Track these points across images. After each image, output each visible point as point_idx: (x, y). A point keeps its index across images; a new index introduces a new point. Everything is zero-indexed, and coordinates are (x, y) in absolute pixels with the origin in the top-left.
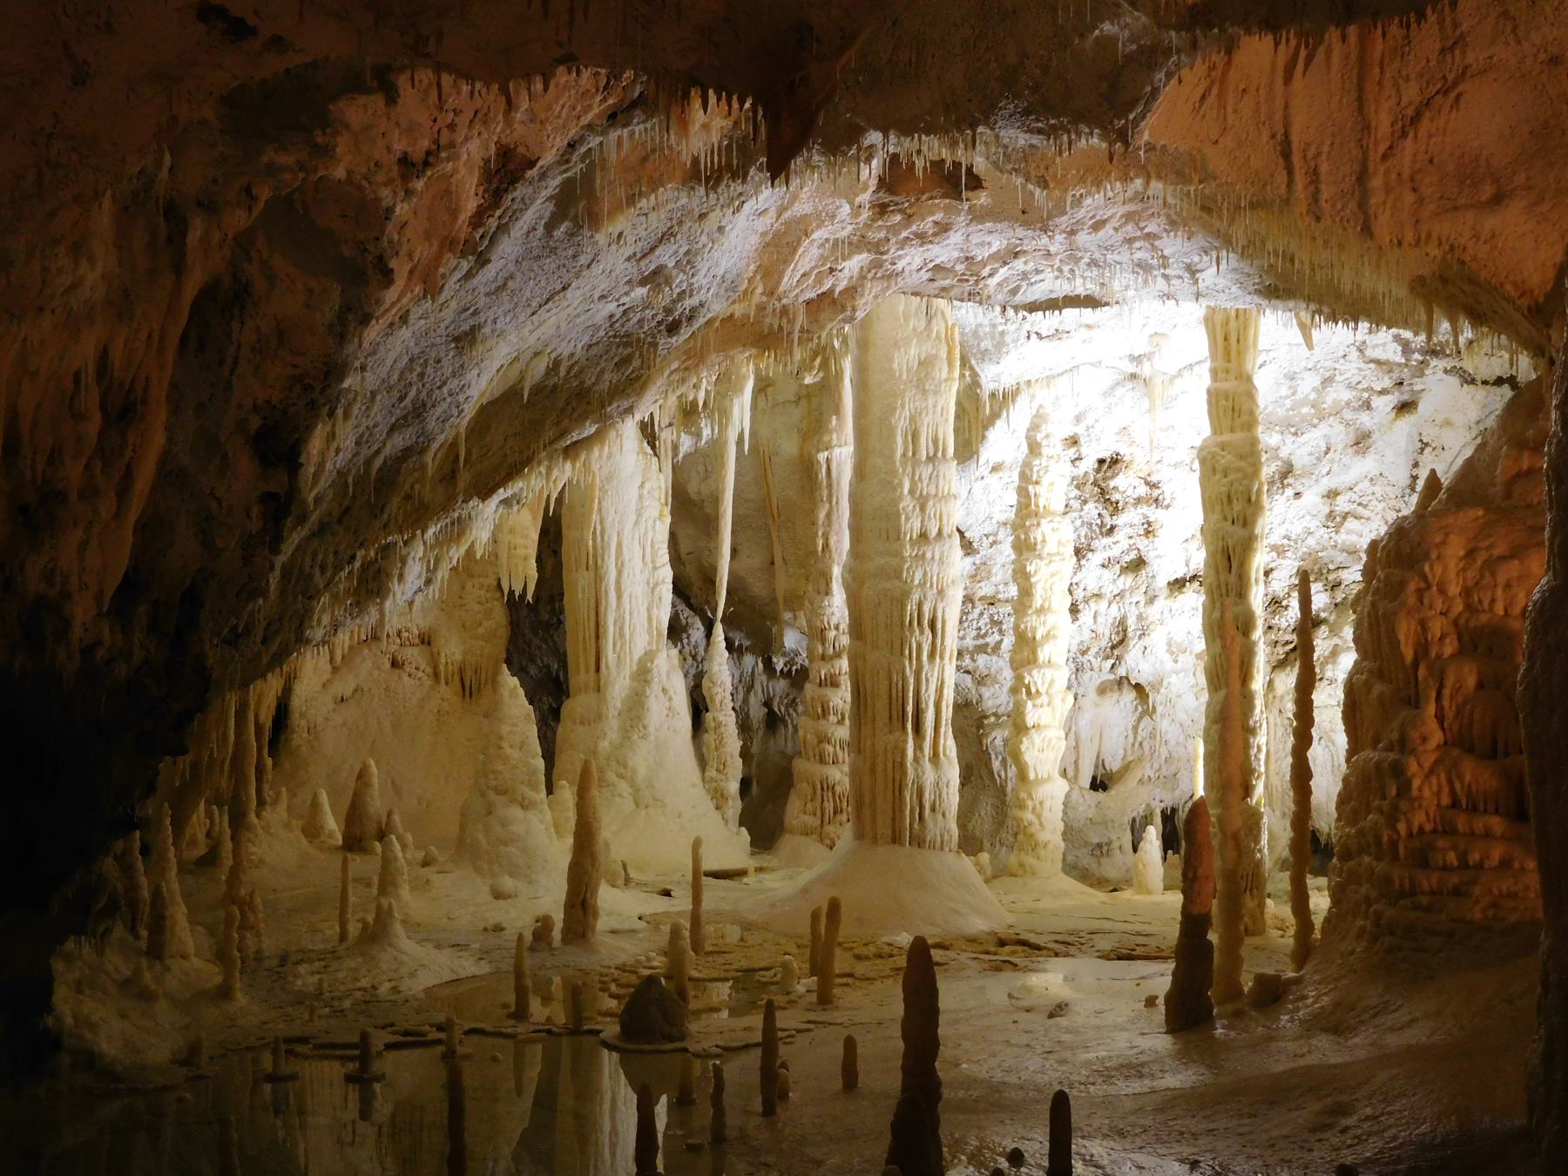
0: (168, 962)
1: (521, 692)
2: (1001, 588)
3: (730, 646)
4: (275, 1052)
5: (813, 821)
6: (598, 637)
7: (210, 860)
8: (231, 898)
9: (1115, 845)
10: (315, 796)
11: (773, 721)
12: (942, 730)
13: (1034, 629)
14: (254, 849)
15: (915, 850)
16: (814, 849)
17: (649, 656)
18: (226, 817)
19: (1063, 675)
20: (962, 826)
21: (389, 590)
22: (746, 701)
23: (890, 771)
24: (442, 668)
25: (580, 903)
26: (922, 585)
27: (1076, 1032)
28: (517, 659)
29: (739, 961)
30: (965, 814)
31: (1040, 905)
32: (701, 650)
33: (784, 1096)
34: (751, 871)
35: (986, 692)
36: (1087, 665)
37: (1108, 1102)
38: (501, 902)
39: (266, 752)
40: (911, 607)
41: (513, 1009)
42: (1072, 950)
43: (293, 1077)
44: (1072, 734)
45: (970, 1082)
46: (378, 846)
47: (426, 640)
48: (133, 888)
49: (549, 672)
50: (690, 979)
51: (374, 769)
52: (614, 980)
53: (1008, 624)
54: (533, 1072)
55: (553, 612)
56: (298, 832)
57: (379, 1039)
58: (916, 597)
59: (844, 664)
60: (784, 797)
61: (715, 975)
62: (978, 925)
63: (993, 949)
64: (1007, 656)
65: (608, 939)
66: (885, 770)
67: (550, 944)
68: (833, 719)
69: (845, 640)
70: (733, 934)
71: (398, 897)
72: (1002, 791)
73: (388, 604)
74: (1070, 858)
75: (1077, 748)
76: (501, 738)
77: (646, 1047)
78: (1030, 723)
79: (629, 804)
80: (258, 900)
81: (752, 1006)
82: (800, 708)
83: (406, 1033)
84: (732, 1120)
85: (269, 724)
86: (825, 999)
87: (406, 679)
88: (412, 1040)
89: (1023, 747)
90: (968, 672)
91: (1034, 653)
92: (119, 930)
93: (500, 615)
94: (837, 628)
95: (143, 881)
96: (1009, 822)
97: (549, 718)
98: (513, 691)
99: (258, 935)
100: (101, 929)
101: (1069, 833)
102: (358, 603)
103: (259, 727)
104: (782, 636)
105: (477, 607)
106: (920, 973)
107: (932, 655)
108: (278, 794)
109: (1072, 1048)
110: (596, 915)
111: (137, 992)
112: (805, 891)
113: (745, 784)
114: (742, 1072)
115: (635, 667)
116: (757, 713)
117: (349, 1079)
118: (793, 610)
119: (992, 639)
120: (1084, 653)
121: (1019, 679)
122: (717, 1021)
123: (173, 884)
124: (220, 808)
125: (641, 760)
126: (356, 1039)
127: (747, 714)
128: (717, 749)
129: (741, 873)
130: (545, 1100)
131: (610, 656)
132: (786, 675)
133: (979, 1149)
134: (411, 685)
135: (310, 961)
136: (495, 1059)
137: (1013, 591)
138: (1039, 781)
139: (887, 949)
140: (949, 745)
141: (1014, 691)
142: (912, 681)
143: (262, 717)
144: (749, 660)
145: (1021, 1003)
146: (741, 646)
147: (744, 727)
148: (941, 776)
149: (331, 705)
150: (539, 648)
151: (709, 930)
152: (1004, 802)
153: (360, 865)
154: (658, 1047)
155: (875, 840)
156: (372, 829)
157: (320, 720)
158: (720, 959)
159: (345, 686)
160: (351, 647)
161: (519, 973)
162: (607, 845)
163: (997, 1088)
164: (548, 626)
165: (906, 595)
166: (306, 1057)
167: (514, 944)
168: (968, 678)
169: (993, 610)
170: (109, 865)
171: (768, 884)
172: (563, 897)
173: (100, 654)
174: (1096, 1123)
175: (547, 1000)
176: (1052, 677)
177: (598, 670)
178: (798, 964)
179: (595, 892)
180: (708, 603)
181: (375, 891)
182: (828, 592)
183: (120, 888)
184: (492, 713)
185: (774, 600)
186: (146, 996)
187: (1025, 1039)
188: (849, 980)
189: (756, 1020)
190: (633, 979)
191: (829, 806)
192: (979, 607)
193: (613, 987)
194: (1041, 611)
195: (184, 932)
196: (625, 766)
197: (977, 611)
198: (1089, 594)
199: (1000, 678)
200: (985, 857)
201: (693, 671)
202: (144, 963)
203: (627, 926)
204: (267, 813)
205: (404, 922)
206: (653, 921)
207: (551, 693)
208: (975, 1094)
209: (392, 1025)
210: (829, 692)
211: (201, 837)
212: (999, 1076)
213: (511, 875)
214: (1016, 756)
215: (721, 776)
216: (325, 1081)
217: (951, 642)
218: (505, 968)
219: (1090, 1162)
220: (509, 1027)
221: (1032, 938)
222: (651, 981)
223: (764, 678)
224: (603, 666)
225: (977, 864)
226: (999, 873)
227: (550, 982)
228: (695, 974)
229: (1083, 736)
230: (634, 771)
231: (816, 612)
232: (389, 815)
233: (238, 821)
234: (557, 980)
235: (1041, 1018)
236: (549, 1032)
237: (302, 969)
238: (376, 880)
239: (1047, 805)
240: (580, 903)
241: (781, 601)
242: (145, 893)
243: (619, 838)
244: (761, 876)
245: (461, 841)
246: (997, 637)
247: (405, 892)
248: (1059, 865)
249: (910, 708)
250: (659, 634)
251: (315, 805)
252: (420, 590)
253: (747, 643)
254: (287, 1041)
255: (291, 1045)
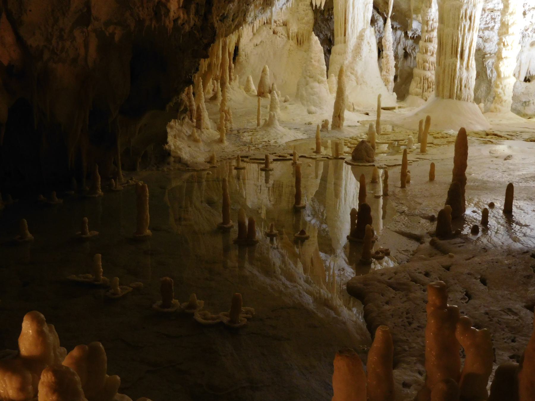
0: (203, 130)
1: (319, 42)
2: (496, 5)
3: (392, 27)
4: (238, 160)
5: (420, 91)
6: (345, 23)
7: (214, 98)
8: (222, 110)
9: (531, 102)
10: (248, 78)
11: (406, 55)
12: (471, 58)
13: (508, 21)
14: (228, 95)
15: (458, 101)
16: (420, 101)
17: (363, 30)
18: (219, 84)
19: (519, 37)
20: (475, 94)
21: (274, 4)
22: (397, 48)
23: (450, 72)
24: (290, 34)
25: (338, 116)
26: (467, 3)
27: (515, 165)
28: (317, 29)
29: (392, 137)
30: (476, 90)
31: (501, 122)
32: (382, 29)
33: (408, 182)
34: (397, 108)
35: (487, 45)
36: (527, 35)
37: (526, 188)
38: (311, 115)
39: (232, 62)
40: (462, 11)
41: (315, 150)
42: (514, 138)
43: (244, 168)
44: (519, 61)
45: (475, 180)
46: (269, 95)
47: (285, 24)
48: (191, 105)
49: (327, 37)
50: (376, 143)
51: (268, 69)
52: (349, 142)
53: (498, 19)
54: (321, 172)
55: (329, 15)
56: (243, 90)
57: (271, 158)
58: (465, 7)
59: (435, 34)
60: (410, 82)
61: (384, 141)
62: (479, 128)
63: (484, 136)
64: (496, 31)
65: (348, 129)
66: (449, 72)
67: (327, 129)
68: (429, 54)
69: (436, 25)
70: (389, 128)
71: (276, 112)
72: (490, 82)
73: (274, 9)
74: (514, 106)
75: (520, 66)
76: (311, 58)
77: (361, 164)
78: (503, 56)
79: (354, 84)
80: (231, 111)
81: (397, 152)
82: (417, 51)
83: (280, 156)
84: (390, 189)
85: (233, 52)
86: (423, 151)
87: (278, 38)
88: (282, 159)
89: (500, 65)
90: (481, 37)
91: (507, 30)
92: (187, 119)
93: (310, 16)
94: (433, 20)
95: (194, 103)
96: (492, 93)
97: (328, 52)
98: (316, 41)
99: (231, 123)
100: (182, 117)
101: (515, 97)
102: (263, 8)
103: (229, 53)
104: (411, 23)
105: (303, 12)
106: (462, 142)
107: (469, 30)
108: (236, 77)
109: (513, 170)
110: (343, 120)
111: (192, 138)
112: (416, 114)
113: (396, 78)
114: (395, 174)
115: (358, 34)
116: (401, 52)
117: (262, 170)
118: (417, 14)
119: (491, 25)
120: (526, 30)
121: (501, 39)
122: (383, 156)
123: (203, 105)
124: (217, 81)
125: (359, 68)
126: (264, 157)
127: (397, 53)
128: (386, 64)
129: (393, 108)
130: (324, 179)
131: (349, 30)
132: (412, 38)
133: (478, 202)
134: (280, 40)
135: (248, 132)
136: (309, 166)
137: (501, 6)
138: (505, 78)
139: (445, 135)
140: (473, 63)
141: (498, 44)
142: (461, 39)
143: (230, 51)
144: (399, 32)
145: (493, 155)
146: (396, 27)
147: (396, 57)
148: (468, 74)
149: (253, 47)
150: (324, 28)
151: (382, 127)
152: (490, 86)
153: (263, 101)
154: (365, 164)
155: (443, 98)
156: (267, 90)
157: (249, 52)
158: (386, 136)
159: (257, 40)
160: (259, 27)
161: (317, 138)
162: (347, 97)
163: (484, 182)
164: (327, 20)
165: (461, 6)
166: (247, 162)
167: (316, 129)
168: (481, 40)
169: (492, 14)
170: (184, 96)
171: (403, 112)
172: (332, 114)
173: (180, 22)
174: (522, 195)
175: (326, 147)
176: (513, 39)
177: (345, 35)
178: (414, 139)
179: (343, 113)
180: (385, 11)
181: (268, 110)
182: (430, 7)
183: (188, 104)
184: (308, 50)
185: (410, 10)
186: (196, 141)
187: (496, 167)
188: (432, 145)
189: (399, 158)
190: (356, 142)
191: (426, 86)
192: (487, 12)
193: (349, 145)
194: (511, 14)
195: (207, 121)
196: (354, 70)
197: (486, 14)
198: (531, 7)
199: (493, 40)
200: (482, 105)
201: (378, 37)
202: (195, 130)
203: (354, 125)
204: (233, 83)
205: (278, 120)
206: (363, 123)
207: (328, 43)
208: (477, 184)
209: (275, 153)
210: (428, 44)
211: (211, 91)
212: (485, 179)
213: (314, 106)
214: (497, 68)
215: (387, 74)
216: (252, 170)
217: (477, 23)
218: (312, 137)
219: (519, 208)
220: (314, 155)
221: (499, 133)
222: (363, 142)
223: (404, 39)
224: (347, 35)
225: (479, 107)
226: (487, 111)
227: (327, 142)
228: (377, 141)
229: (523, 62)
230: (357, 72)
231: (425, 14)
232: (273, 85)
233: (223, 85)
234: (329, 141)
235: (502, 160)
236: (327, 158)
237: (245, 134)
238: (269, 106)
239: (507, 86)
240: (338, 116)
241: (412, 11)
242: (195, 107)
243: (352, 95)
244: (400, 109)
245: (297, 94)
246: (493, 24)
247: (278, 110)
248: (510, 108)
249: (459, 49)
250: (367, 22)
251: (248, 81)
252: (285, 4)
253: (398, 26)
254: (242, 157)
255: (243, 158)
